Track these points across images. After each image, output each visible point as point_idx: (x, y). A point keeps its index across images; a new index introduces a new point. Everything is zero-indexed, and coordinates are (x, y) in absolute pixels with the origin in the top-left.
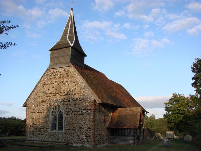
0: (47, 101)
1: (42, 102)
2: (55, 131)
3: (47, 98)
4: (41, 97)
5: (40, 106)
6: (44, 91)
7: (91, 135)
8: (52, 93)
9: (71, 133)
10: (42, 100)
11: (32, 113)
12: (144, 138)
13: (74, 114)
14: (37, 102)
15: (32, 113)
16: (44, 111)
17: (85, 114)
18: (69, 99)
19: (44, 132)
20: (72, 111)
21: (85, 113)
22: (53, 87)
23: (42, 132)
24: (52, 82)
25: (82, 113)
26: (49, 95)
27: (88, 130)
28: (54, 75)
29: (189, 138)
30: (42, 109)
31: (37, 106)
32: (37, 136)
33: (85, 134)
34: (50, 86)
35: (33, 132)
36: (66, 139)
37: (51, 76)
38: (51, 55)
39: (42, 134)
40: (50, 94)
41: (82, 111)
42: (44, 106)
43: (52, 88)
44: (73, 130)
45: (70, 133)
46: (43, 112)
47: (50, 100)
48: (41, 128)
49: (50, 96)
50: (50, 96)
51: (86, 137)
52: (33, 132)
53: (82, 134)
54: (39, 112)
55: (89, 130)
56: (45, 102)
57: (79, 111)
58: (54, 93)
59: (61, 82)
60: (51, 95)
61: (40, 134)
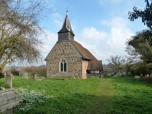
1: (55, 58)
5: (54, 60)
8: (60, 54)
13: (72, 64)
55: (80, 71)
56: (56, 58)
60: (59, 55)
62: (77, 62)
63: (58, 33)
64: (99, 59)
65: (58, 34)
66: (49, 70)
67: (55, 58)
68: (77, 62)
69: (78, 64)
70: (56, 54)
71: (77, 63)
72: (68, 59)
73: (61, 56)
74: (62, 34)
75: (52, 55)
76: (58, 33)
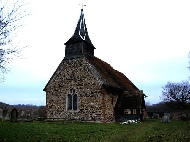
4: (59, 83)
6: (60, 77)
8: (67, 80)
13: (87, 96)
15: (51, 96)
19: (61, 112)
27: (98, 110)
31: (55, 90)
32: (56, 115)
33: (96, 113)
37: (66, 65)
39: (60, 114)
40: (66, 80)
42: (61, 90)
44: (86, 109)
45: (83, 113)
46: (61, 95)
51: (97, 115)
56: (62, 87)
58: (69, 79)
60: (66, 81)
61: (58, 113)
62: (96, 92)
68: (96, 92)
69: (96, 96)
73: (69, 82)
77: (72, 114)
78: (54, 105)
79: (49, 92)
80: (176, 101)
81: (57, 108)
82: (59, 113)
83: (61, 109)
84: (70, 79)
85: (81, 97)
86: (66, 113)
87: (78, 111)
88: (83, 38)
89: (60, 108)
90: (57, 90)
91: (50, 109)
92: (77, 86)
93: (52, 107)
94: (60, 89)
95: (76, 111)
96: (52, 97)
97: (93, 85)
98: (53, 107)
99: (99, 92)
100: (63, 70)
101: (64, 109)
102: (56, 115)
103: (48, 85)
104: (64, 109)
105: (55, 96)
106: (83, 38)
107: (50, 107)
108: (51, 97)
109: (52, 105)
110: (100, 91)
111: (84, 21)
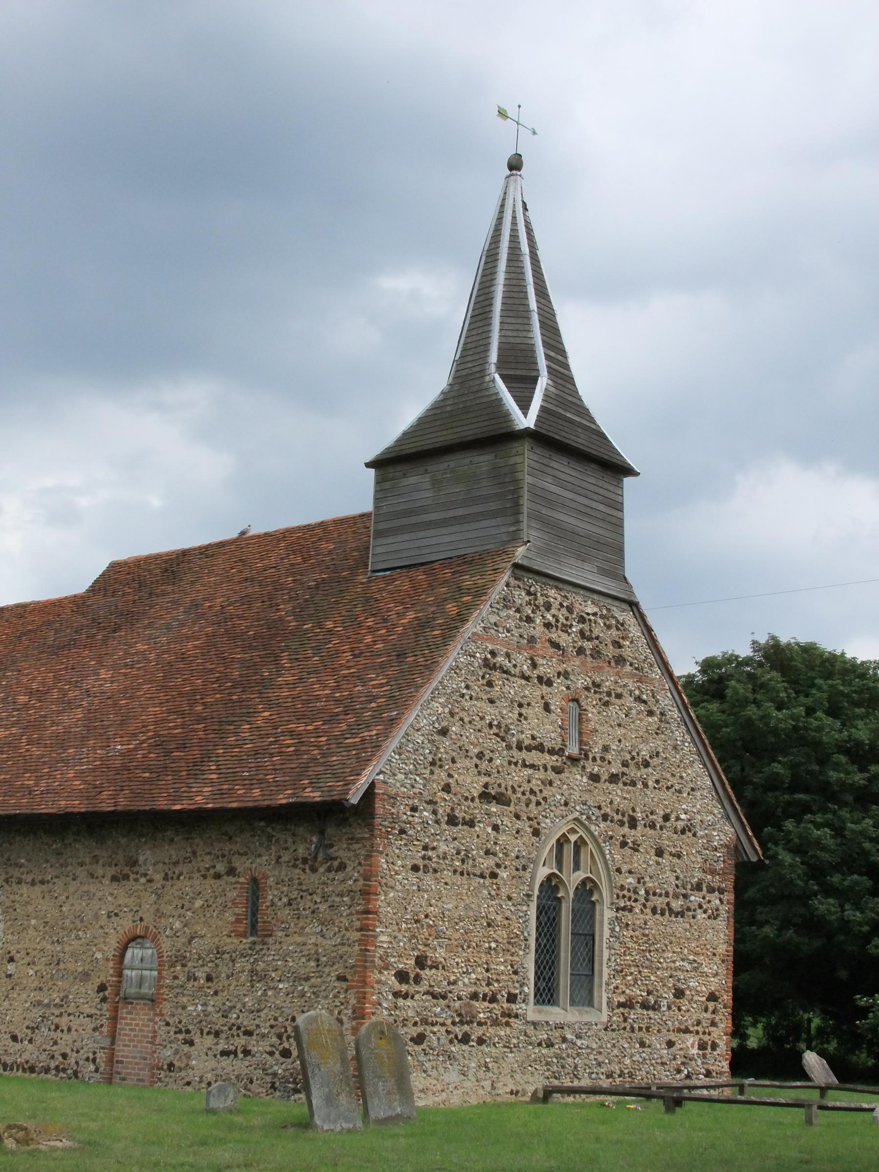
0: (514, 798)
1: (485, 796)
2: (555, 1014)
3: (518, 776)
4: (480, 756)
5: (471, 824)
6: (491, 713)
7: (720, 1038)
8: (540, 748)
9: (640, 1029)
10: (485, 779)
11: (415, 868)
12: (134, 939)
13: (654, 911)
14: (447, 788)
15: (415, 868)
16: (498, 866)
17: (700, 915)
18: (634, 810)
19: (496, 1023)
20: (647, 892)
21: (700, 907)
22: (547, 708)
23: (480, 1024)
24: (541, 671)
25: (689, 909)
26: (524, 754)
27: (706, 1010)
28: (548, 625)
29: (431, 967)
30: (487, 852)
31: (452, 821)
32: (450, 1057)
33: (697, 1033)
34: (533, 692)
35: (425, 1021)
36: (616, 1068)
37: (529, 620)
38: (378, 483)
39: (481, 1041)
40: (529, 749)
41: (685, 896)
42: (496, 828)
43: (538, 708)
44: (645, 1006)
45: (632, 1029)
46: (494, 875)
47: (532, 792)
48: (474, 996)
49: (532, 766)
50: (532, 766)
51: (702, 1046)
52: (425, 1021)
53: (687, 1031)
54: (468, 866)
55: (711, 1005)
56: (501, 799)
57: (676, 896)
58: (552, 752)
59: (587, 689)
60: (533, 757)
61: (465, 1039)
62: (698, 887)
63: (368, 465)
64: (233, 534)
65: (379, 482)
66: (402, 976)
67: (485, 796)
68: (698, 887)
69: (700, 915)
70: (502, 732)
71: (695, 898)
72: (624, 844)
73: (551, 775)
74: (391, 471)
75: (444, 732)
76: (368, 465)
77: (564, 1040)
78: (440, 954)
79: (402, 831)
80: (790, 1011)
81: (464, 988)
82: (477, 1032)
83: (493, 999)
84: (560, 752)
85: (624, 909)
86: (530, 1030)
87: (605, 1019)
88: (525, 407)
89: (484, 989)
90: (465, 823)
91: (406, 996)
92: (605, 817)
93: (417, 980)
94: (489, 814)
95: (593, 1020)
96: (429, 880)
97: (683, 832)
98: (426, 973)
99: (711, 890)
100: (508, 655)
101: (512, 998)
102: (450, 1057)
103: (707, 773)
104: (512, 998)
105: (447, 874)
106: (525, 407)
107: (402, 976)
108: (413, 877)
109: (421, 962)
110: (716, 881)
111: (525, 248)
